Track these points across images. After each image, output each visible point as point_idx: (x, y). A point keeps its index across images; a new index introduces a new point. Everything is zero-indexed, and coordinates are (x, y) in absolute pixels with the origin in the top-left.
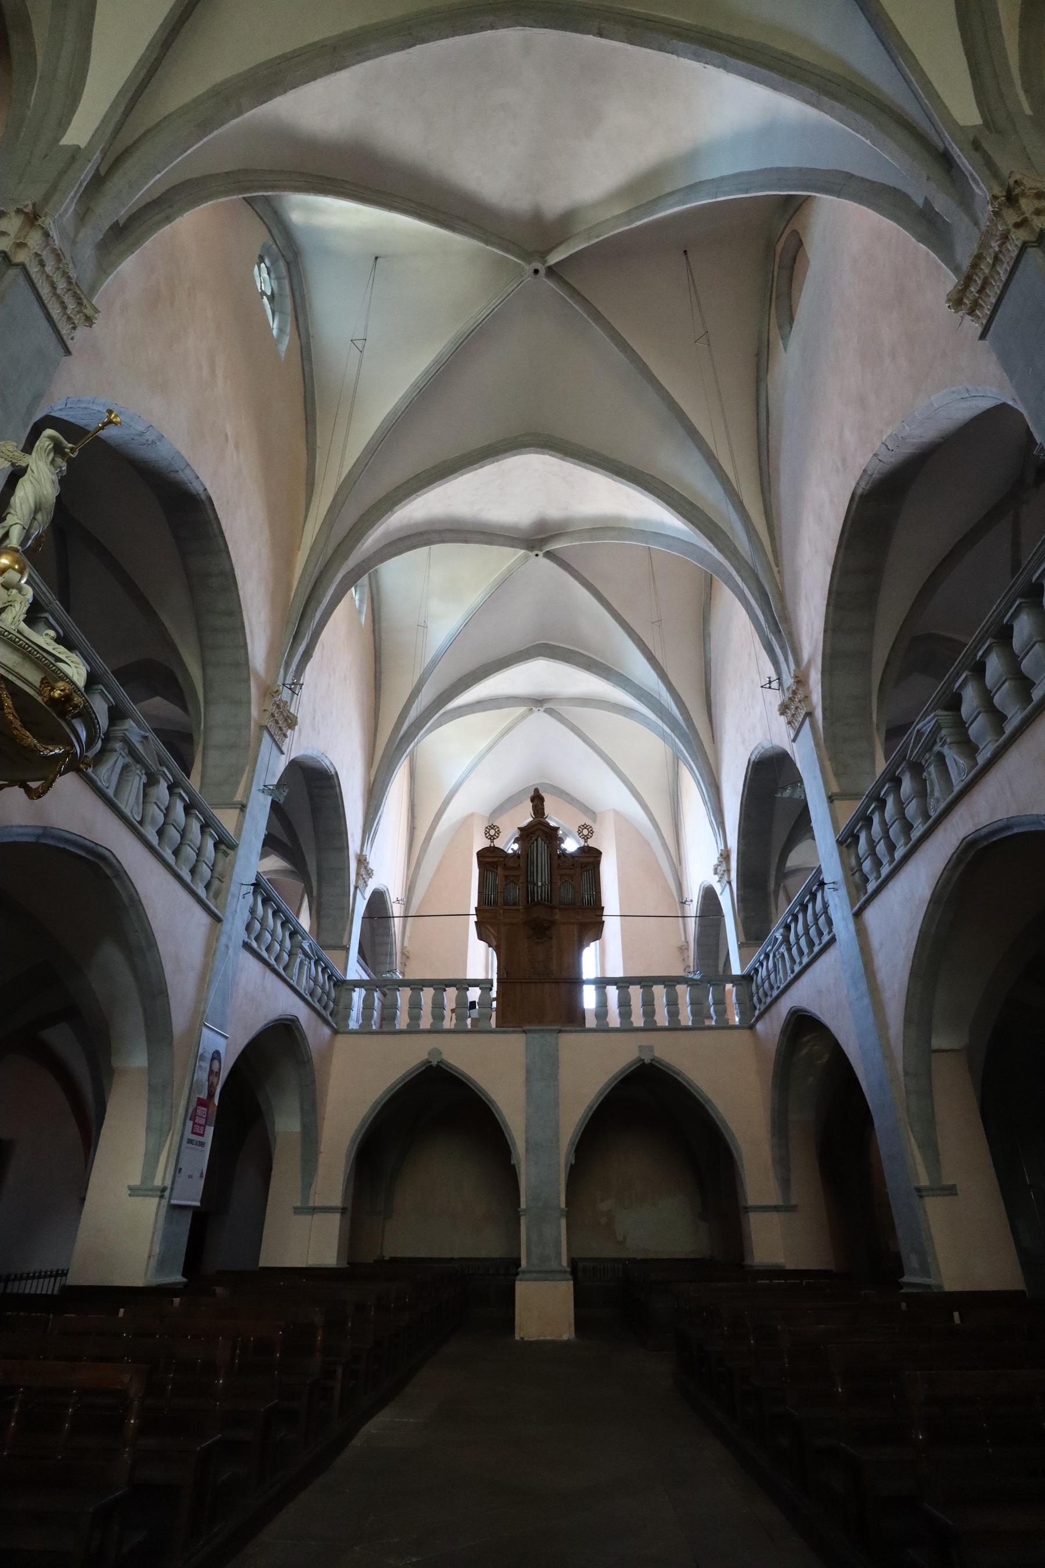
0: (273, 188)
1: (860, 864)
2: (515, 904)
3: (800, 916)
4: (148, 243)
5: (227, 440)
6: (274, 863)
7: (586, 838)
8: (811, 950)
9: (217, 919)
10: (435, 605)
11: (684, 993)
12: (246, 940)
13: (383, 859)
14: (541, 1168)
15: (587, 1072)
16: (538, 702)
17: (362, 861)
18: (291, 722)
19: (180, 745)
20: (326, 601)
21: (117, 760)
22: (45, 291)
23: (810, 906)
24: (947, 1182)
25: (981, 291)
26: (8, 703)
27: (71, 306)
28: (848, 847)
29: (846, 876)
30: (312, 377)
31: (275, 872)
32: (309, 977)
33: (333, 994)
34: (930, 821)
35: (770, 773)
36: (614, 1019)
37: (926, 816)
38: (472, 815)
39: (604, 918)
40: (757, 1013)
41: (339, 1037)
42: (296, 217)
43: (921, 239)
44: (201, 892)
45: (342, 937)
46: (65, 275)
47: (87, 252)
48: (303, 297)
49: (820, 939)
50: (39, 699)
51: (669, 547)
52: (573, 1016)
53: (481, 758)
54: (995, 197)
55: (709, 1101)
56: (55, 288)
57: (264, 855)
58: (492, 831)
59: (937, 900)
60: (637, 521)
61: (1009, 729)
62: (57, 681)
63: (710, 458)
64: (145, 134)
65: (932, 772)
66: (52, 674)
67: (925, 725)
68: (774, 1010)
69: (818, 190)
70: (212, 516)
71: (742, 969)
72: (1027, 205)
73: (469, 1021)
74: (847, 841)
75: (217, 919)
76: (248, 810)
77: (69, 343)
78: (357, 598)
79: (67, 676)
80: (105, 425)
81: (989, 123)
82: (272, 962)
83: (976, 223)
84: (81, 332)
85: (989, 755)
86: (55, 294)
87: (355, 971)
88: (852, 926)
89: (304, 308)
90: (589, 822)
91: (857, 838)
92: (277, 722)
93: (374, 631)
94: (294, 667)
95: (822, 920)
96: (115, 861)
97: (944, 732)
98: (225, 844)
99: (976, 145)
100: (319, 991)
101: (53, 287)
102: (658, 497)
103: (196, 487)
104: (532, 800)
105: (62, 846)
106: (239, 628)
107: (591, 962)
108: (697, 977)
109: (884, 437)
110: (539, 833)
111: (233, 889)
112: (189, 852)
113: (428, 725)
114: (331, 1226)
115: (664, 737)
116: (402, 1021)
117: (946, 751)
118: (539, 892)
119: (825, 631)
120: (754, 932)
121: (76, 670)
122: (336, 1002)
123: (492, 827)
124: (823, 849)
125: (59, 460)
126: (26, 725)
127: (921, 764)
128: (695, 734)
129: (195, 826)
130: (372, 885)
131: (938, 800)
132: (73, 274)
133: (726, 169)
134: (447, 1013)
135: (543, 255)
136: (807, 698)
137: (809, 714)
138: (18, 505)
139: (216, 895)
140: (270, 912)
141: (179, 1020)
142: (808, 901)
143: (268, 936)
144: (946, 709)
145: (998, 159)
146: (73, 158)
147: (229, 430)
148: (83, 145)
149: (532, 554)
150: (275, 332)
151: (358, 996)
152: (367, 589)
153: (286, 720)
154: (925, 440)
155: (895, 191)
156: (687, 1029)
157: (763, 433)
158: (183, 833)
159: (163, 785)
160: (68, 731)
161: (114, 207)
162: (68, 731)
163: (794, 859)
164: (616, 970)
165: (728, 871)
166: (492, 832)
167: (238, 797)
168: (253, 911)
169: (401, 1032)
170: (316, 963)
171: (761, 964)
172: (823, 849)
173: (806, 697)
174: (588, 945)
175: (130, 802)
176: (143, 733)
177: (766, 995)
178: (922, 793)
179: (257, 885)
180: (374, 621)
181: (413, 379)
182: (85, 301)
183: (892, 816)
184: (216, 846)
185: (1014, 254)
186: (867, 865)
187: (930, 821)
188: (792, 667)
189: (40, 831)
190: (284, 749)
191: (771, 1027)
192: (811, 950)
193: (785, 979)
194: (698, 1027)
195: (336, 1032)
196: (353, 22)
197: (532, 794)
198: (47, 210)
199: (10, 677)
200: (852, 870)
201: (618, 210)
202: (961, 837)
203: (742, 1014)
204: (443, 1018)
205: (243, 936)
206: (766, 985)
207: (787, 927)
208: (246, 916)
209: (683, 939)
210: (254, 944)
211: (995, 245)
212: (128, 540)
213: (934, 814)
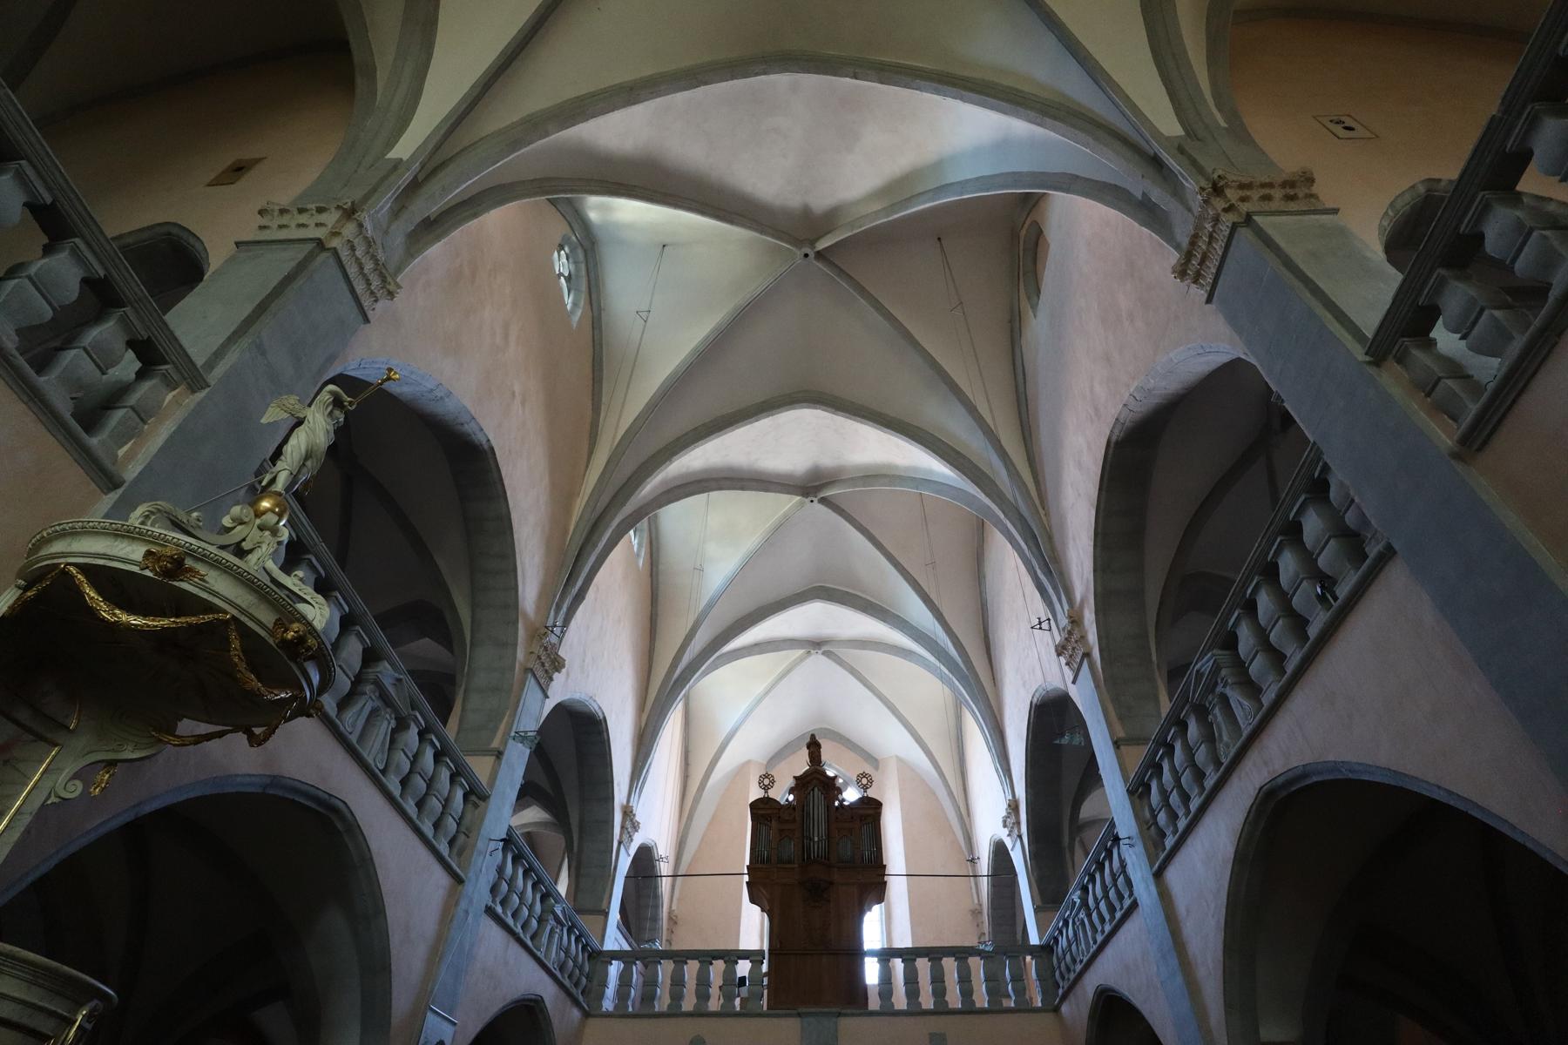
0: (572, 191)
1: (1155, 817)
2: (789, 862)
3: (1098, 876)
4: (456, 233)
6: (534, 815)
7: (865, 788)
8: (1113, 917)
9: (459, 880)
10: (712, 549)
11: (977, 965)
13: (653, 812)
16: (816, 644)
17: (628, 813)
18: (558, 664)
19: (440, 691)
20: (601, 545)
21: (366, 703)
22: (352, 271)
25: (1202, 263)
26: (236, 644)
27: (376, 283)
28: (1140, 797)
29: (1141, 832)
31: (535, 824)
32: (560, 947)
33: (587, 968)
35: (1052, 715)
36: (900, 1001)
37: (1218, 763)
38: (749, 762)
41: (591, 1021)
42: (593, 216)
43: (1144, 223)
44: (443, 848)
45: (601, 900)
46: (374, 258)
47: (398, 238)
48: (597, 278)
50: (271, 641)
51: (937, 492)
52: (854, 993)
53: (759, 701)
54: (1202, 189)
58: (767, 781)
59: (1242, 859)
60: (907, 469)
61: (1290, 667)
63: (972, 410)
65: (1217, 714)
67: (1204, 664)
68: (1078, 989)
69: (1056, 189)
73: (737, 1001)
74: (1139, 791)
75: (459, 880)
76: (505, 757)
77: (370, 314)
79: (304, 618)
81: (1190, 133)
82: (519, 930)
83: (1190, 210)
88: (1153, 888)
89: (598, 286)
90: (869, 770)
94: (565, 609)
95: (1121, 880)
97: (1224, 672)
98: (476, 795)
99: (1181, 150)
101: (361, 268)
107: (873, 930)
110: (815, 783)
111: (480, 845)
112: (435, 804)
115: (942, 678)
116: (663, 1002)
117: (1228, 692)
118: (815, 846)
120: (1049, 898)
124: (1113, 797)
126: (253, 668)
128: (975, 675)
129: (445, 775)
130: (638, 840)
132: (381, 256)
133: (969, 175)
135: (812, 243)
136: (1083, 638)
137: (1087, 655)
139: (460, 854)
140: (520, 872)
141: (401, 1002)
144: (1223, 648)
145: (1202, 160)
147: (517, 388)
149: (807, 500)
151: (614, 969)
152: (646, 535)
156: (983, 1011)
158: (430, 783)
159: (414, 730)
161: (427, 205)
163: (1087, 810)
164: (904, 940)
165: (1018, 823)
166: (766, 782)
167: (495, 744)
168: (500, 870)
169: (661, 1015)
170: (570, 931)
172: (1113, 797)
175: (373, 752)
177: (1069, 970)
178: (1210, 738)
179: (508, 842)
184: (466, 797)
186: (1162, 818)
189: (268, 781)
191: (1077, 1009)
192: (1113, 917)
194: (995, 1010)
195: (587, 1015)
196: (647, 71)
199: (243, 618)
201: (877, 207)
203: (1044, 993)
204: (708, 997)
205: (486, 898)
206: (1068, 957)
207: (1085, 889)
208: (492, 876)
210: (499, 909)
211: (1208, 226)
213: (1225, 761)
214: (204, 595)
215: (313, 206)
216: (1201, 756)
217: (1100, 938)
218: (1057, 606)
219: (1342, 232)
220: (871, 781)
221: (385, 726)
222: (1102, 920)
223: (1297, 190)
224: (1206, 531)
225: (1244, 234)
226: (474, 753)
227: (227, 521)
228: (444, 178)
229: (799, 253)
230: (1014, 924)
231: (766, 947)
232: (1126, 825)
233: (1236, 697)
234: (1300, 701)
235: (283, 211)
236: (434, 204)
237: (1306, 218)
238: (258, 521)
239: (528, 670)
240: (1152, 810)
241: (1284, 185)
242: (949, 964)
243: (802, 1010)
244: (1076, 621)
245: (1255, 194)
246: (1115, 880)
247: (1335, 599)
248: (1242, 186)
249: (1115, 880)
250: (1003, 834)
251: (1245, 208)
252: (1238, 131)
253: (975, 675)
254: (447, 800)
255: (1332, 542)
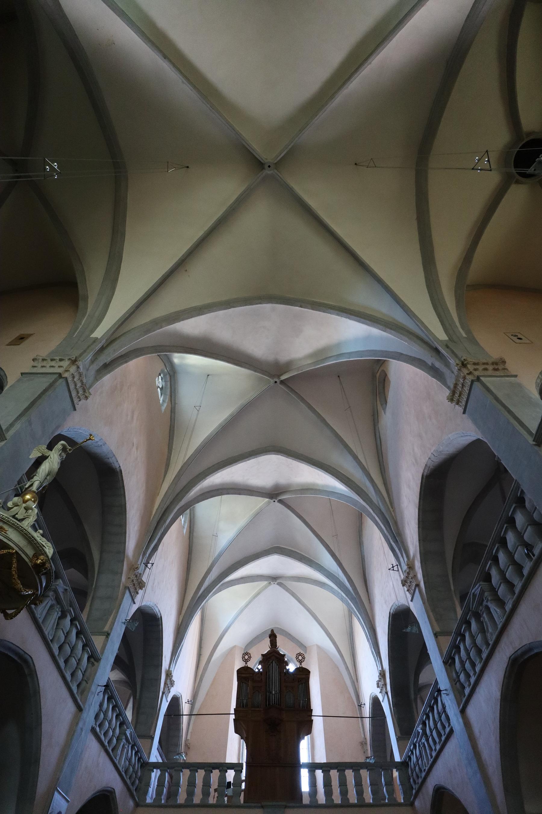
0: (170, 351)
1: (458, 677)
3: (431, 715)
5: (133, 445)
6: (116, 676)
7: (301, 662)
12: (94, 725)
13: (181, 678)
16: (274, 579)
17: (169, 675)
18: (141, 585)
19: (81, 594)
21: (48, 602)
22: (72, 387)
23: (435, 707)
25: (460, 396)
27: (81, 392)
28: (450, 665)
30: (174, 420)
32: (126, 758)
33: (139, 774)
34: (490, 646)
35: (401, 619)
36: (321, 798)
37: (488, 644)
38: (235, 647)
39: (313, 718)
40: (414, 791)
44: (74, 688)
46: (82, 381)
47: (92, 372)
49: (445, 732)
50: (30, 564)
54: (457, 364)
56: (76, 386)
57: (112, 669)
58: (246, 657)
60: (323, 486)
62: (40, 555)
63: (355, 458)
64: (123, 334)
66: (39, 550)
67: (476, 590)
68: (424, 790)
69: (391, 358)
70: (120, 479)
71: (401, 759)
72: (471, 367)
73: (226, 799)
74: (449, 662)
75: (80, 709)
76: (110, 637)
77: (76, 406)
78: (183, 520)
79: (46, 553)
80: (87, 440)
81: (451, 339)
82: (106, 744)
84: (83, 401)
85: (510, 606)
86: (76, 388)
88: (461, 720)
91: (454, 660)
92: (134, 585)
93: (190, 538)
96: (32, 664)
97: (486, 594)
98: (94, 658)
99: (447, 347)
100: (131, 769)
101: (76, 385)
102: (333, 475)
103: (116, 465)
104: (270, 637)
105: (6, 653)
106: (123, 533)
107: (307, 750)
108: (372, 761)
109: (432, 451)
110: (273, 658)
111: (93, 688)
113: (214, 590)
115: (342, 599)
117: (489, 604)
118: (273, 698)
119: (419, 540)
120: (405, 731)
121: (49, 550)
122: (140, 780)
123: (246, 654)
124: (437, 670)
125: (63, 454)
126: (19, 577)
127: (478, 612)
128: (360, 599)
129: (80, 645)
131: (491, 634)
132: (84, 381)
134: (212, 790)
135: (279, 376)
136: (415, 576)
137: (418, 585)
138: (41, 472)
139: (82, 693)
142: (433, 704)
143: (107, 724)
146: (94, 342)
147: (135, 441)
148: (99, 338)
150: (161, 402)
151: (155, 775)
152: (188, 516)
153: (139, 584)
154: (450, 452)
155: (420, 360)
156: (369, 805)
157: (379, 447)
158: (73, 649)
159: (69, 618)
160: (38, 581)
161: (106, 358)
162: (38, 581)
163: (423, 678)
164: (321, 758)
165: (385, 685)
166: (246, 657)
167: (106, 629)
168: (101, 705)
169: (180, 806)
170: (132, 748)
171: (412, 753)
172: (437, 670)
173: (415, 576)
174: (303, 738)
175: (48, 630)
176: (65, 587)
177: (418, 777)
178: (483, 630)
180: (190, 532)
181: (220, 422)
182: (87, 391)
183: (470, 646)
184: (89, 658)
185: (469, 384)
186: (462, 677)
187: (490, 646)
188: (406, 559)
190: (135, 600)
193: (428, 764)
195: (137, 805)
197: (270, 633)
198: (80, 359)
199: (20, 552)
200: (455, 680)
201: (309, 361)
202: (508, 656)
203: (405, 793)
206: (417, 768)
207: (424, 724)
208: (97, 708)
209: (363, 736)
211: (461, 380)
212: (85, 490)
213: (491, 643)
214: (5, 540)
215: (58, 358)
216: (479, 640)
217: (434, 754)
218: (401, 559)
219: (520, 386)
220: (304, 658)
221: (56, 615)
222: (435, 742)
223: (499, 365)
224: (469, 520)
225: (476, 385)
226: (94, 634)
227: (10, 504)
228: (115, 345)
229: (272, 381)
230: (385, 751)
231: (244, 760)
232: (444, 683)
233: (493, 607)
234: (524, 609)
235: (43, 360)
236: (109, 357)
237: (503, 379)
238: (24, 505)
239: (127, 588)
240: (457, 673)
241: (493, 364)
242: (350, 774)
244: (411, 567)
245: (481, 367)
246: (440, 717)
247: (534, 555)
248: (475, 364)
249: (440, 717)
250: (377, 692)
251: (476, 373)
252: (472, 340)
253: (360, 599)
254: (79, 660)
255: (529, 527)
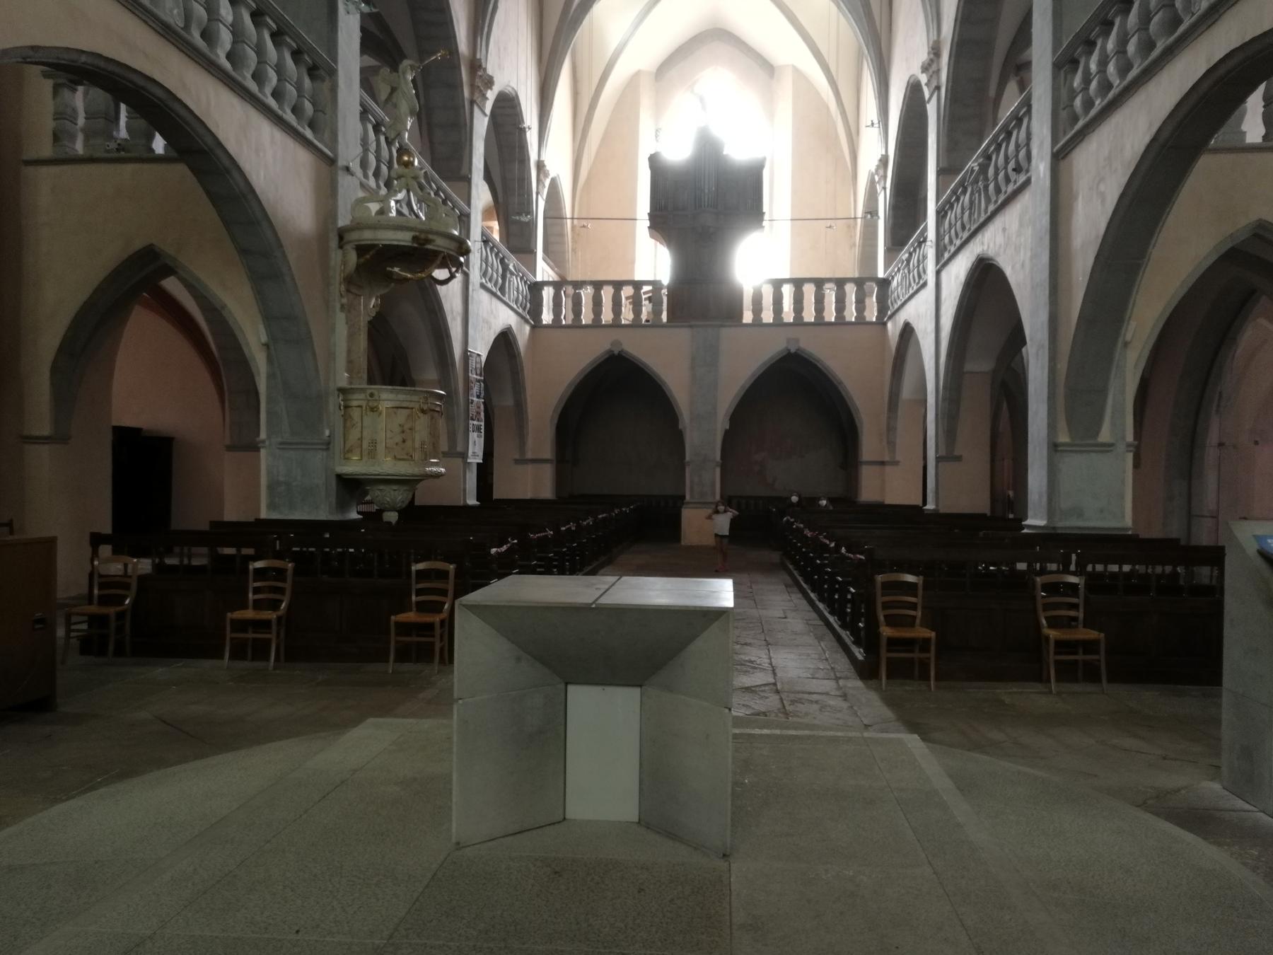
14: (704, 433)
15: (740, 366)
17: (540, 166)
24: (956, 453)
55: (841, 383)
87: (544, 271)
95: (1022, 153)
114: (548, 472)
118: (702, 206)
207: (911, 254)
243: (693, 323)
